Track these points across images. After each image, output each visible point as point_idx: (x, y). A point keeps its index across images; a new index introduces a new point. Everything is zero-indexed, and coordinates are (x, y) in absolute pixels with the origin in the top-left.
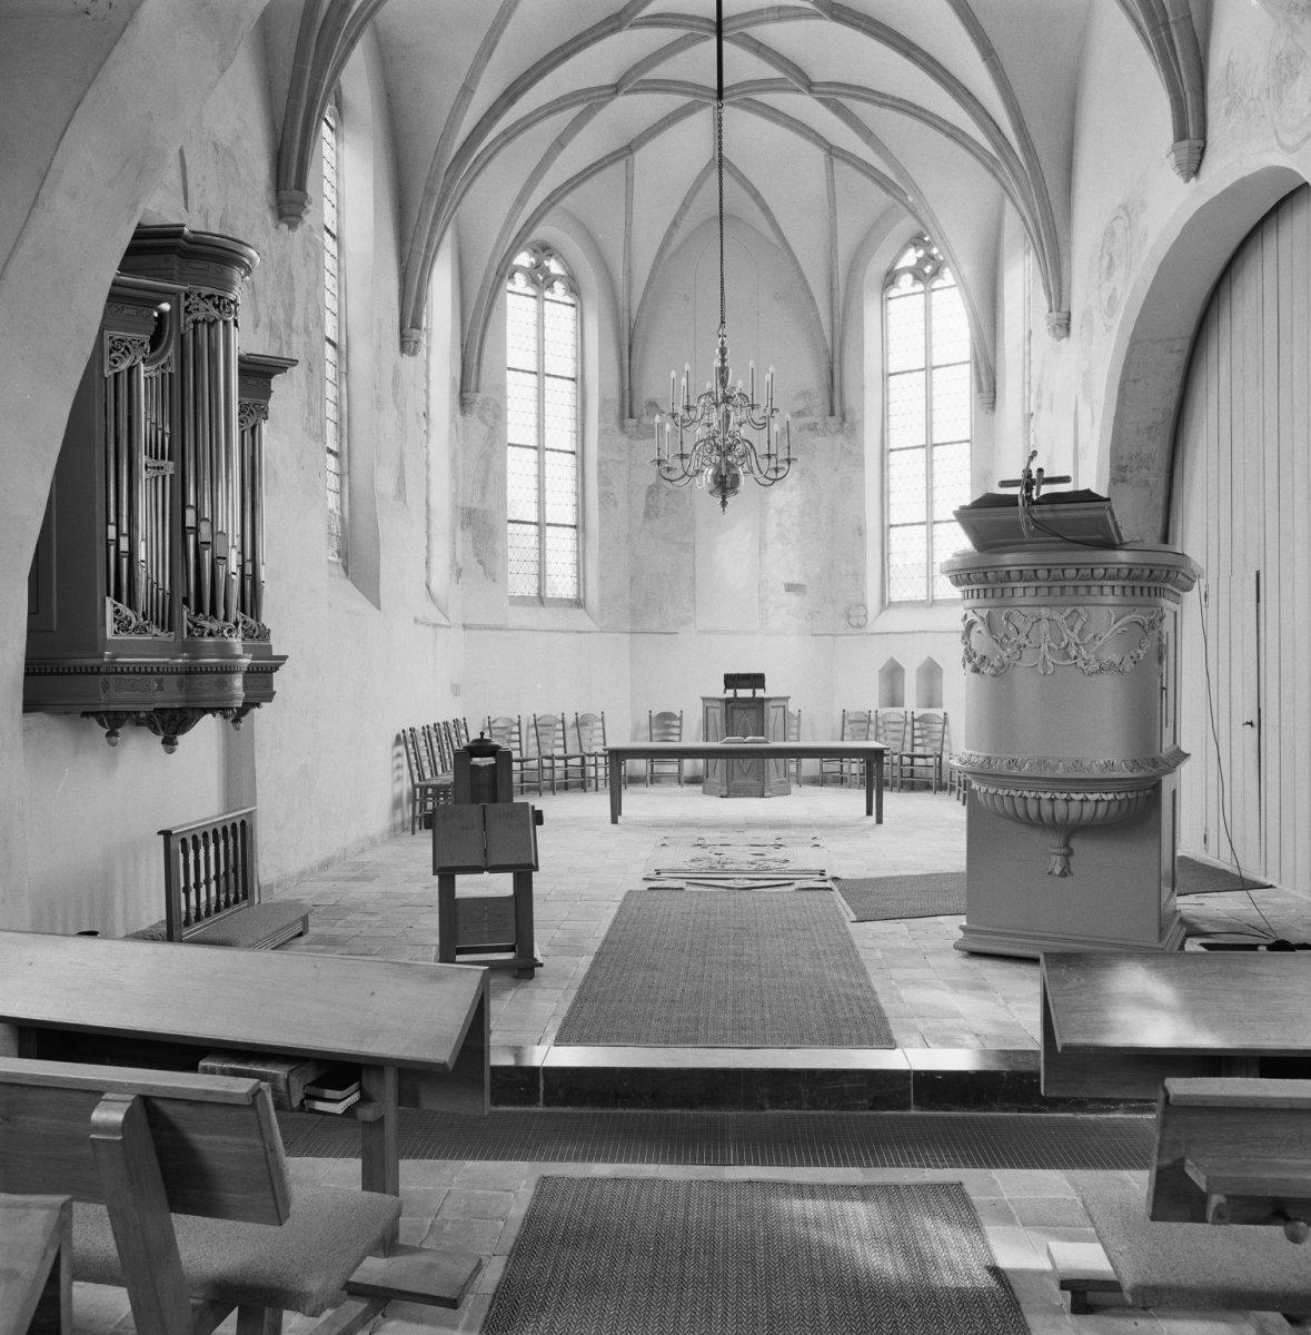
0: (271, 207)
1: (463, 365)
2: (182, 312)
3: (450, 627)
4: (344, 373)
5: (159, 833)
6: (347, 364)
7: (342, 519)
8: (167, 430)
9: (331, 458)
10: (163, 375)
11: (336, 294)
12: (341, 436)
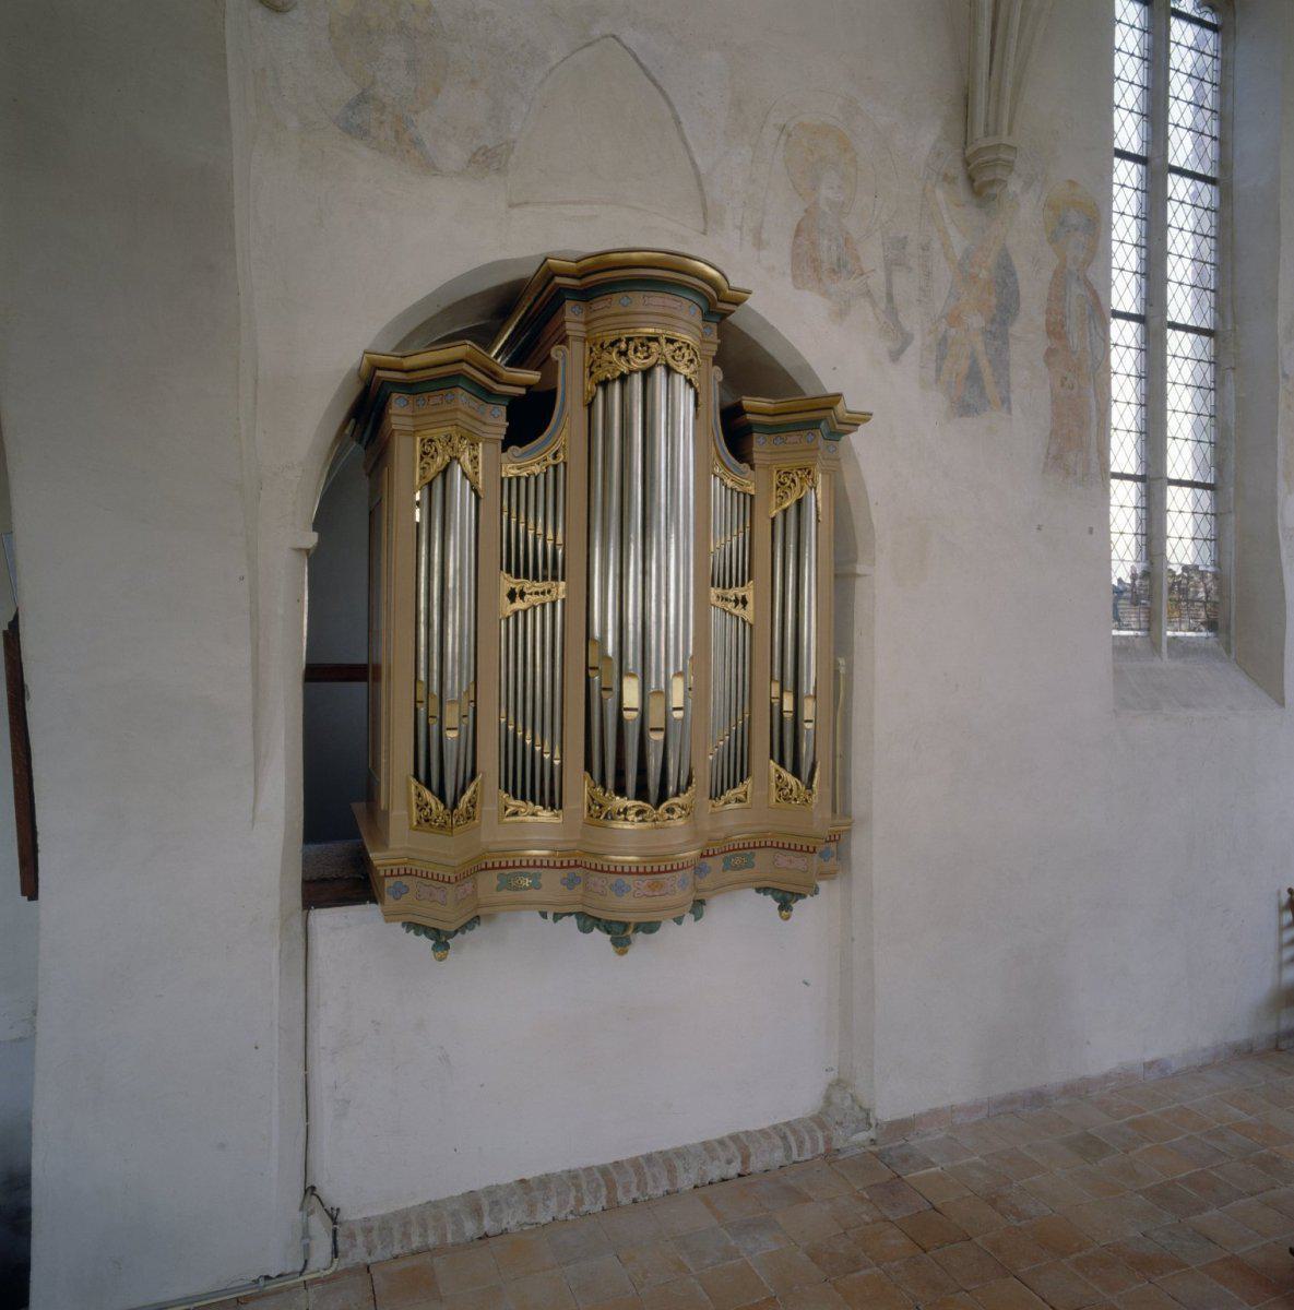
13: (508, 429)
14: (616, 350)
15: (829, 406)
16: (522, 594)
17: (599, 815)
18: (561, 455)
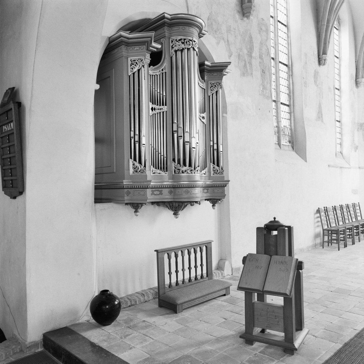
0: (238, 12)
1: (356, 69)
2: (171, 47)
3: (350, 168)
4: (291, 74)
5: (155, 251)
6: (292, 72)
7: (291, 129)
8: (164, 94)
9: (274, 103)
10: (162, 73)
11: (287, 47)
12: (290, 99)
13: (150, 61)
14: (181, 42)
15: (329, 57)
16: (155, 109)
17: (177, 171)
18: (164, 70)
